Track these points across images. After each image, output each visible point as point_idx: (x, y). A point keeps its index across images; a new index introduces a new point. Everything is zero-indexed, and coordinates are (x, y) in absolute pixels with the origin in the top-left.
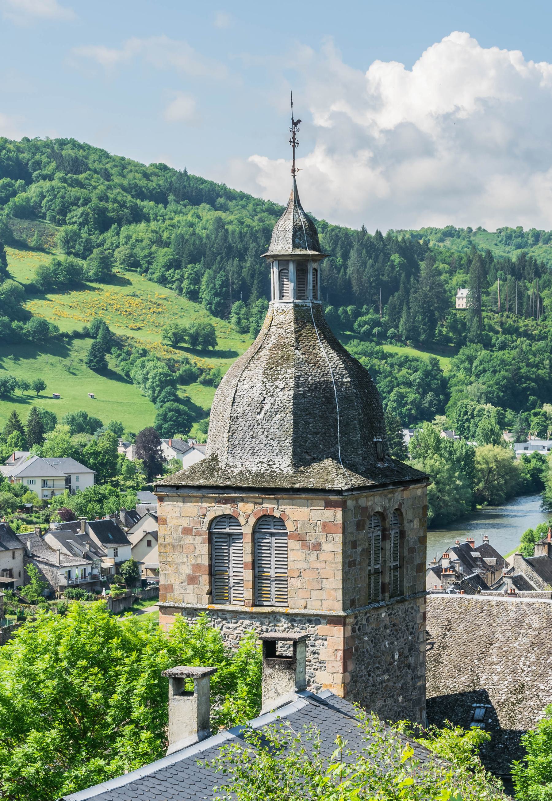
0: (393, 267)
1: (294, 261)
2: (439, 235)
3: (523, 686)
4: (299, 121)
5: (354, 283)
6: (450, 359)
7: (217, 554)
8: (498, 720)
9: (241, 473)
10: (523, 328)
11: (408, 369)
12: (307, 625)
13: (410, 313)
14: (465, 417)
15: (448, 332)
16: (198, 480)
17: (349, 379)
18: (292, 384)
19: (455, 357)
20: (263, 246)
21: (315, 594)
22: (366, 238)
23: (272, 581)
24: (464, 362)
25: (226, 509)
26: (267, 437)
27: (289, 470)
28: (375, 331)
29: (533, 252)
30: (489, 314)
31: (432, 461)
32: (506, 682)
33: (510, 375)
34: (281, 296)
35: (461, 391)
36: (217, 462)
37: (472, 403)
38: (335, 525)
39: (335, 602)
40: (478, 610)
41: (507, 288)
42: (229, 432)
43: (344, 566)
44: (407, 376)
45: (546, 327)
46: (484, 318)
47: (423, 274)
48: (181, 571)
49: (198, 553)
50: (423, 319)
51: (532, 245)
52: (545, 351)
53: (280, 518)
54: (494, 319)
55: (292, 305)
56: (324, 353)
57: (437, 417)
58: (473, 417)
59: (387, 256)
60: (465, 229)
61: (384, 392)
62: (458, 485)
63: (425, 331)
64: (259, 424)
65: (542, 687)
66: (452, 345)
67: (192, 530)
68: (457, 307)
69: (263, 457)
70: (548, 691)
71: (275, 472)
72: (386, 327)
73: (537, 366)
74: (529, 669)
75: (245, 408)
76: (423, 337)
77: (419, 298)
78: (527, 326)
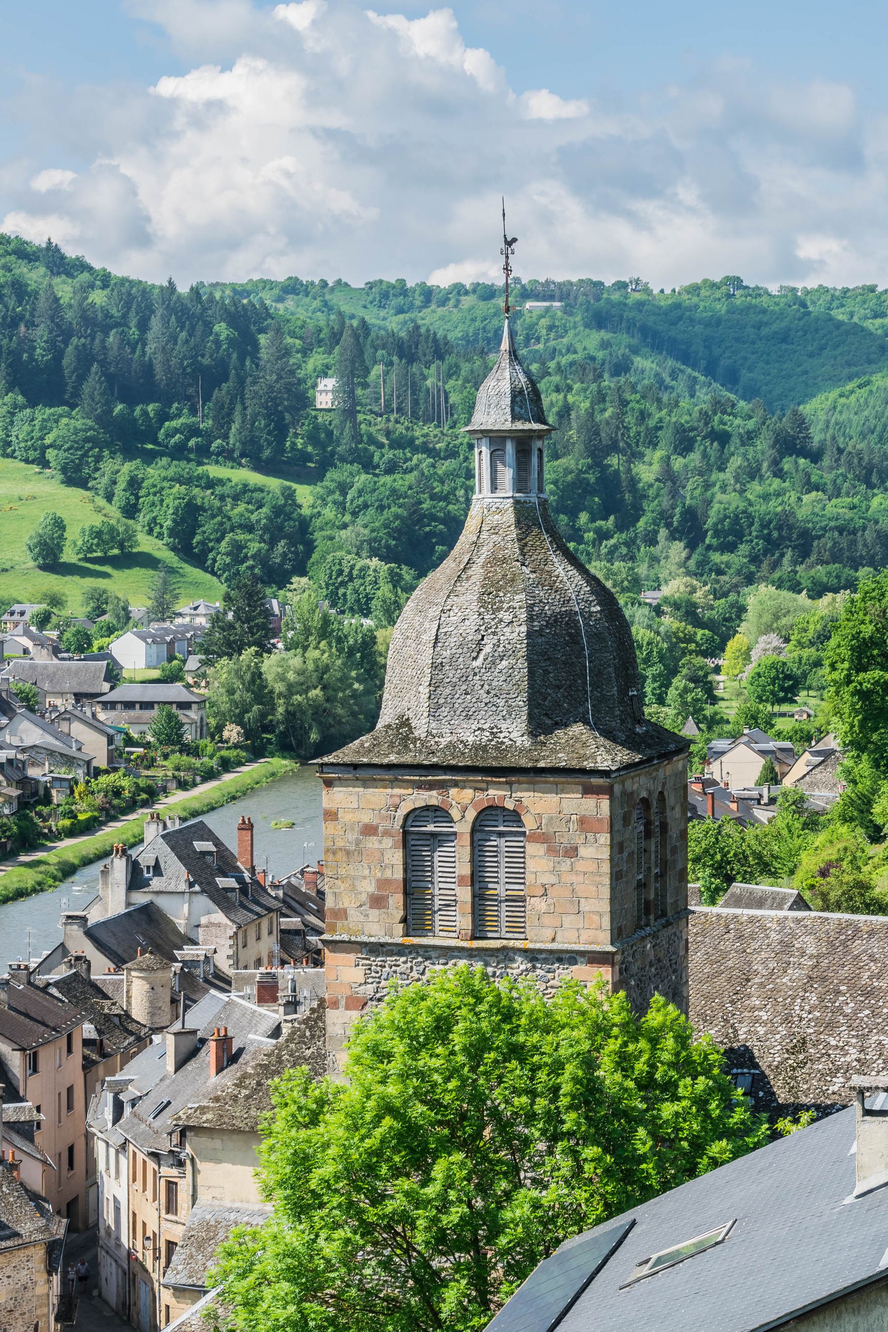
0: (218, 343)
1: (512, 438)
2: (276, 291)
3: (804, 1043)
4: (514, 240)
5: (158, 369)
6: (311, 488)
7: (415, 863)
8: (774, 1093)
9: (451, 746)
10: (422, 439)
11: (248, 503)
12: (557, 965)
13: (246, 415)
14: (340, 579)
15: (305, 445)
16: (387, 755)
17: (598, 608)
18: (523, 617)
19: (319, 484)
20: (14, 309)
21: (568, 920)
22: (174, 298)
23: (501, 902)
24: (333, 492)
25: (432, 797)
26: (488, 693)
27: (525, 742)
28: (192, 443)
29: (423, 319)
30: (368, 417)
31: (317, 653)
32: (778, 1036)
33: (405, 513)
34: (494, 488)
35: (331, 538)
36: (410, 728)
37: (349, 557)
38: (598, 820)
39: (599, 932)
40: (722, 929)
41: (394, 377)
42: (430, 685)
43: (611, 879)
44: (247, 515)
45: (457, 437)
46: (361, 423)
47: (264, 354)
48: (360, 889)
49: (386, 861)
50: (267, 426)
51: (420, 310)
52: (458, 476)
53: (514, 811)
54: (376, 425)
55: (511, 500)
56: (560, 571)
57: (295, 579)
58: (351, 579)
59: (209, 326)
60: (317, 282)
61: (211, 541)
62: (356, 690)
63: (269, 443)
64: (475, 674)
65: (833, 1043)
66: (312, 465)
67: (376, 828)
68: (319, 407)
69: (483, 721)
70: (842, 1048)
71: (503, 743)
72: (209, 437)
73: (445, 498)
74: (810, 1016)
75: (454, 651)
76: (267, 453)
77: (261, 392)
78: (425, 436)
